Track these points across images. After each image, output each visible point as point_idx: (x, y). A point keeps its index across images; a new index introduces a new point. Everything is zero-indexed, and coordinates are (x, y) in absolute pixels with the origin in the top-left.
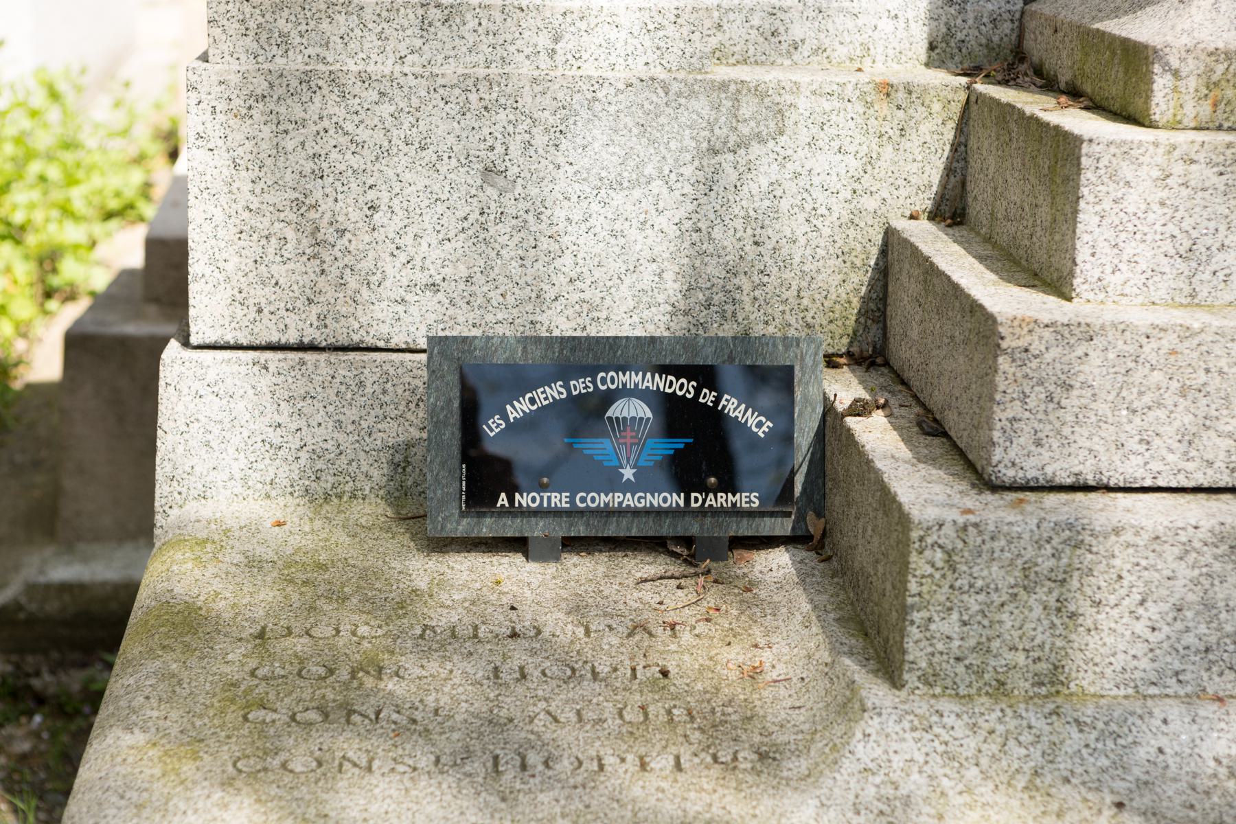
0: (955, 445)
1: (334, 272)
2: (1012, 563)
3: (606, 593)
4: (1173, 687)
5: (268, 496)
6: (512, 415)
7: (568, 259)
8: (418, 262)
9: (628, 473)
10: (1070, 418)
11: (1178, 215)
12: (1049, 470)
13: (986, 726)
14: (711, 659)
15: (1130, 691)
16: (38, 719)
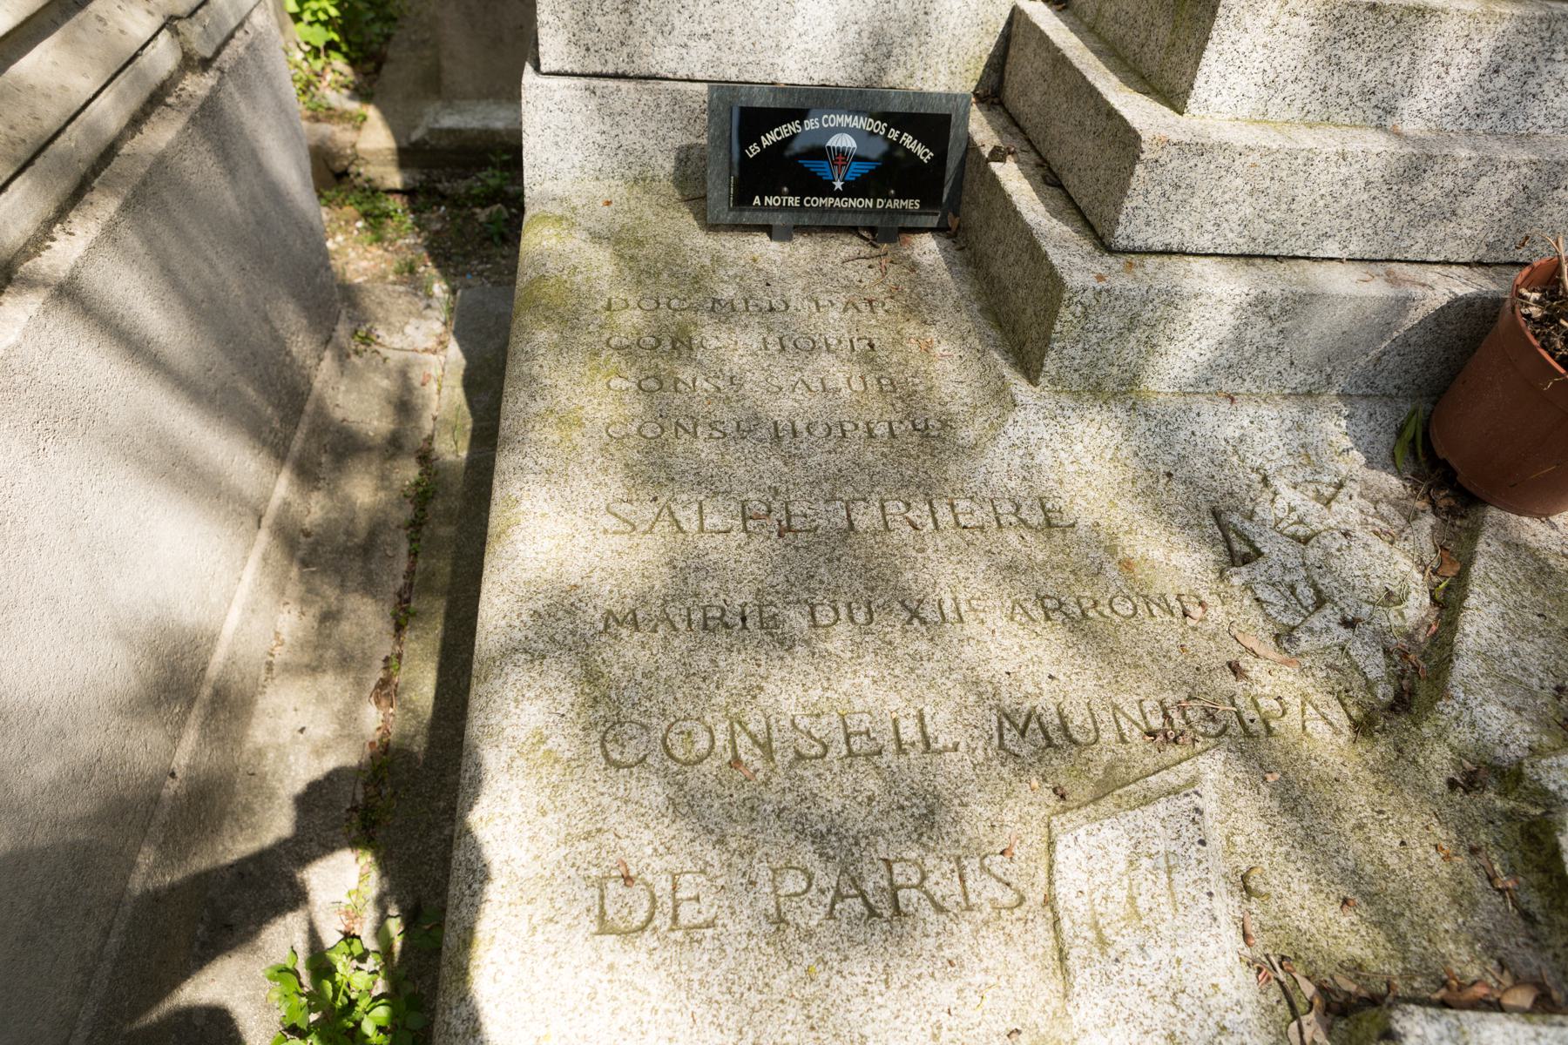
0: (1070, 199)
1: (638, 23)
2: (1124, 315)
3: (825, 271)
4: (1203, 386)
5: (597, 179)
6: (765, 143)
7: (799, 19)
8: (696, 17)
9: (838, 185)
10: (1173, 208)
11: (1273, 55)
12: (1150, 242)
13: (1090, 416)
14: (898, 333)
15: (1176, 390)
16: (443, 208)
